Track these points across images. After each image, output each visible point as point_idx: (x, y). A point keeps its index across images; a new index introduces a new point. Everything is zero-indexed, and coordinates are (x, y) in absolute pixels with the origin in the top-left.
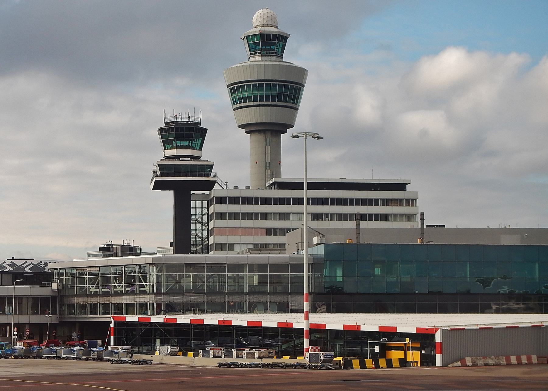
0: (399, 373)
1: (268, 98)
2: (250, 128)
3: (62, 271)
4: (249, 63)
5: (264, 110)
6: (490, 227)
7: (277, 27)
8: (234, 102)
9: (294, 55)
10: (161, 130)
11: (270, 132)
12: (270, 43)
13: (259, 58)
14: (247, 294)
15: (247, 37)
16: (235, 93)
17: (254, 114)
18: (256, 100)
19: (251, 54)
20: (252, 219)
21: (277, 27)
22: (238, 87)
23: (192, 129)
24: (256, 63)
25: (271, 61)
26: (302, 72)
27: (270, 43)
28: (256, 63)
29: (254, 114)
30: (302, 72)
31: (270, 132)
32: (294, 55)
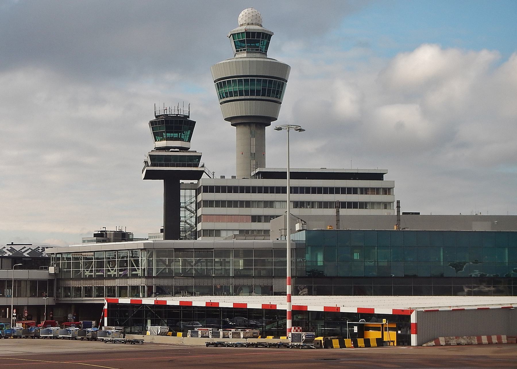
0: (377, 352)
1: (252, 93)
2: (236, 121)
3: (58, 256)
4: (235, 60)
5: (249, 104)
6: (462, 214)
7: (261, 26)
8: (221, 97)
9: (278, 52)
10: (152, 123)
11: (255, 125)
12: (254, 41)
13: (245, 55)
14: (233, 277)
15: (233, 35)
16: (221, 87)
17: (240, 108)
18: (241, 95)
19: (237, 51)
20: (237, 207)
21: (261, 26)
22: (224, 82)
23: (181, 122)
24: (241, 60)
25: (256, 58)
26: (285, 68)
27: (254, 41)
28: (241, 60)
29: (240, 108)
30: (285, 68)
31: (255, 125)
32: (278, 52)
